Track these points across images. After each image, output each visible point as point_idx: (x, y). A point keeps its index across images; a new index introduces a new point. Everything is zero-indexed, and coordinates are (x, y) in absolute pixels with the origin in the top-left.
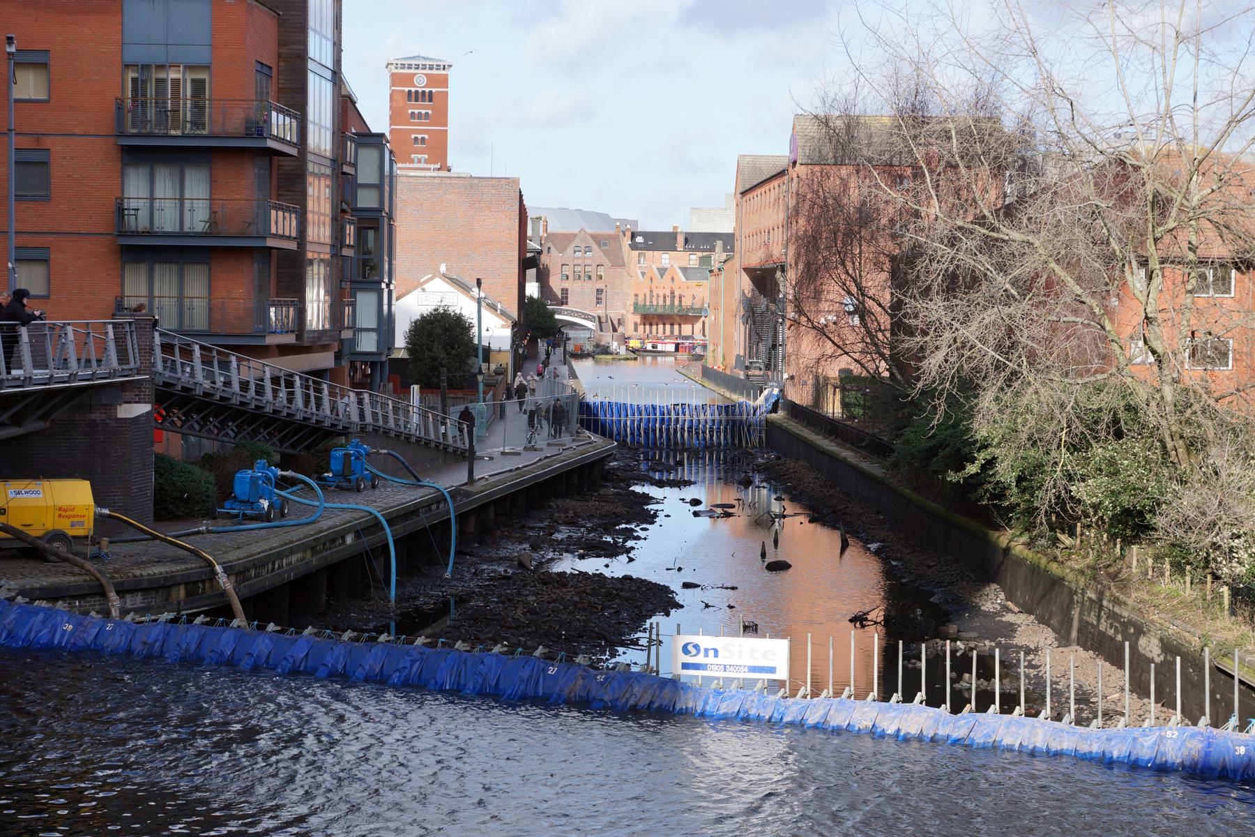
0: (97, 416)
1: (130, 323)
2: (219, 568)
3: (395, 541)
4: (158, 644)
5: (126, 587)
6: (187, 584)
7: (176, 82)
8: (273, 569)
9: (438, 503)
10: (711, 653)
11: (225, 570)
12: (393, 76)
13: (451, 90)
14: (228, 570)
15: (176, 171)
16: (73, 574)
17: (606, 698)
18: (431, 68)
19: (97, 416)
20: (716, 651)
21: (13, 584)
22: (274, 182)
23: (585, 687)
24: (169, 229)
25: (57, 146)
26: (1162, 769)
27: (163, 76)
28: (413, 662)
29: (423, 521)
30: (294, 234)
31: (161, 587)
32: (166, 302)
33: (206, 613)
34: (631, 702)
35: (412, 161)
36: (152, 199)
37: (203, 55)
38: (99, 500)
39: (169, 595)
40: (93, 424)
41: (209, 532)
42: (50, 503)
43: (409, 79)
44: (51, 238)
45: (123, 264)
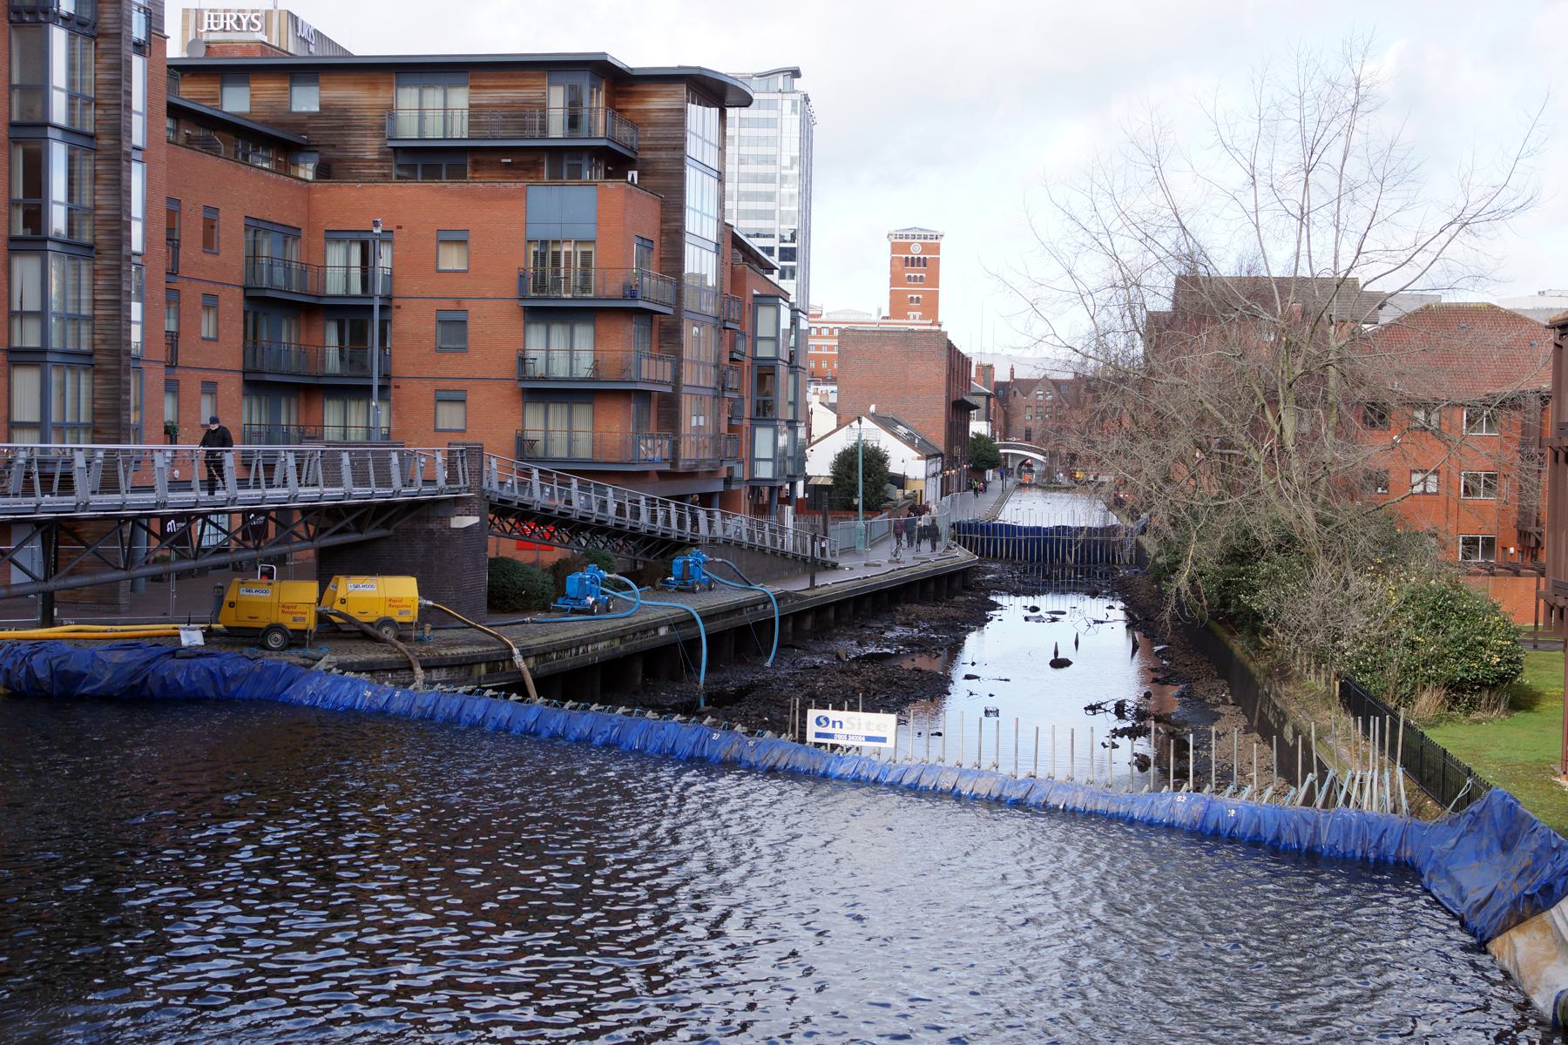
0: (433, 526)
1: (462, 451)
2: (516, 651)
3: (707, 637)
4: (430, 709)
5: (432, 664)
6: (487, 663)
7: (568, 254)
8: (577, 654)
9: (766, 603)
10: (837, 724)
11: (522, 652)
12: (893, 245)
13: (943, 256)
14: (526, 654)
15: (567, 328)
16: (390, 652)
17: (752, 760)
18: (925, 238)
19: (433, 526)
20: (841, 723)
21: (334, 658)
22: (655, 336)
23: (739, 750)
24: (561, 375)
25: (472, 307)
26: (1170, 828)
27: (556, 249)
28: (613, 727)
29: (747, 618)
30: (668, 379)
31: (467, 664)
32: (558, 435)
33: (494, 689)
34: (771, 763)
35: (908, 318)
36: (548, 350)
37: (588, 232)
38: (423, 592)
39: (471, 672)
40: (431, 532)
41: (532, 622)
42: (383, 596)
43: (906, 248)
44: (467, 382)
45: (525, 403)
